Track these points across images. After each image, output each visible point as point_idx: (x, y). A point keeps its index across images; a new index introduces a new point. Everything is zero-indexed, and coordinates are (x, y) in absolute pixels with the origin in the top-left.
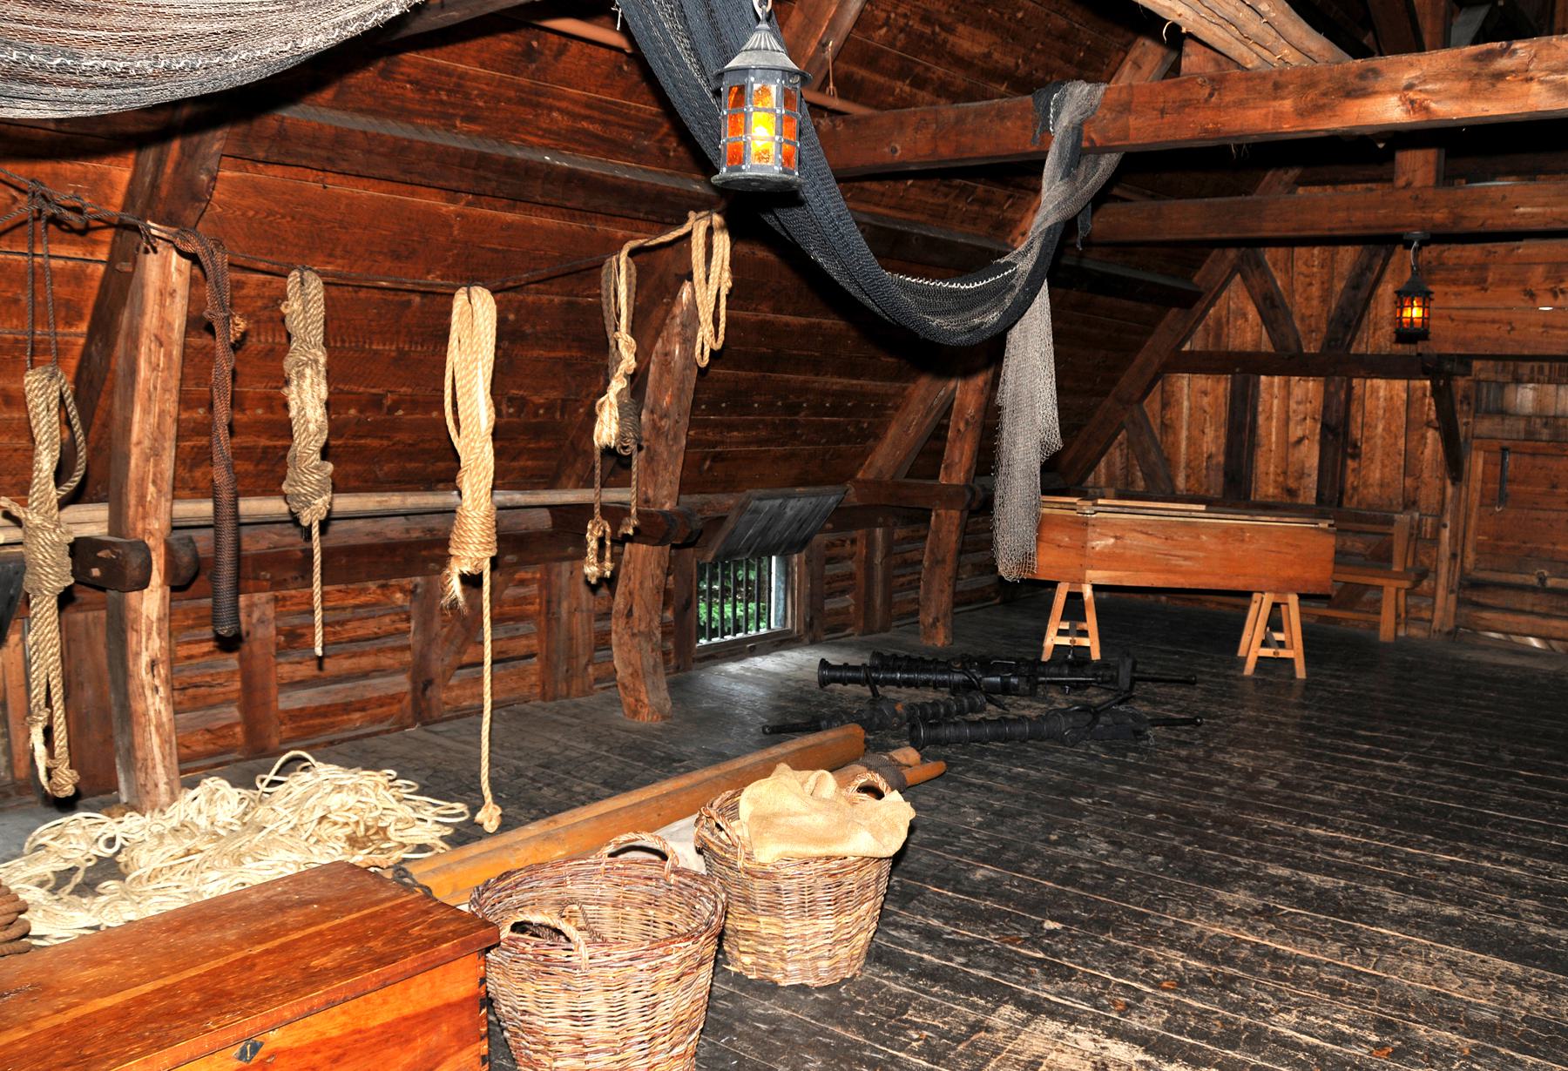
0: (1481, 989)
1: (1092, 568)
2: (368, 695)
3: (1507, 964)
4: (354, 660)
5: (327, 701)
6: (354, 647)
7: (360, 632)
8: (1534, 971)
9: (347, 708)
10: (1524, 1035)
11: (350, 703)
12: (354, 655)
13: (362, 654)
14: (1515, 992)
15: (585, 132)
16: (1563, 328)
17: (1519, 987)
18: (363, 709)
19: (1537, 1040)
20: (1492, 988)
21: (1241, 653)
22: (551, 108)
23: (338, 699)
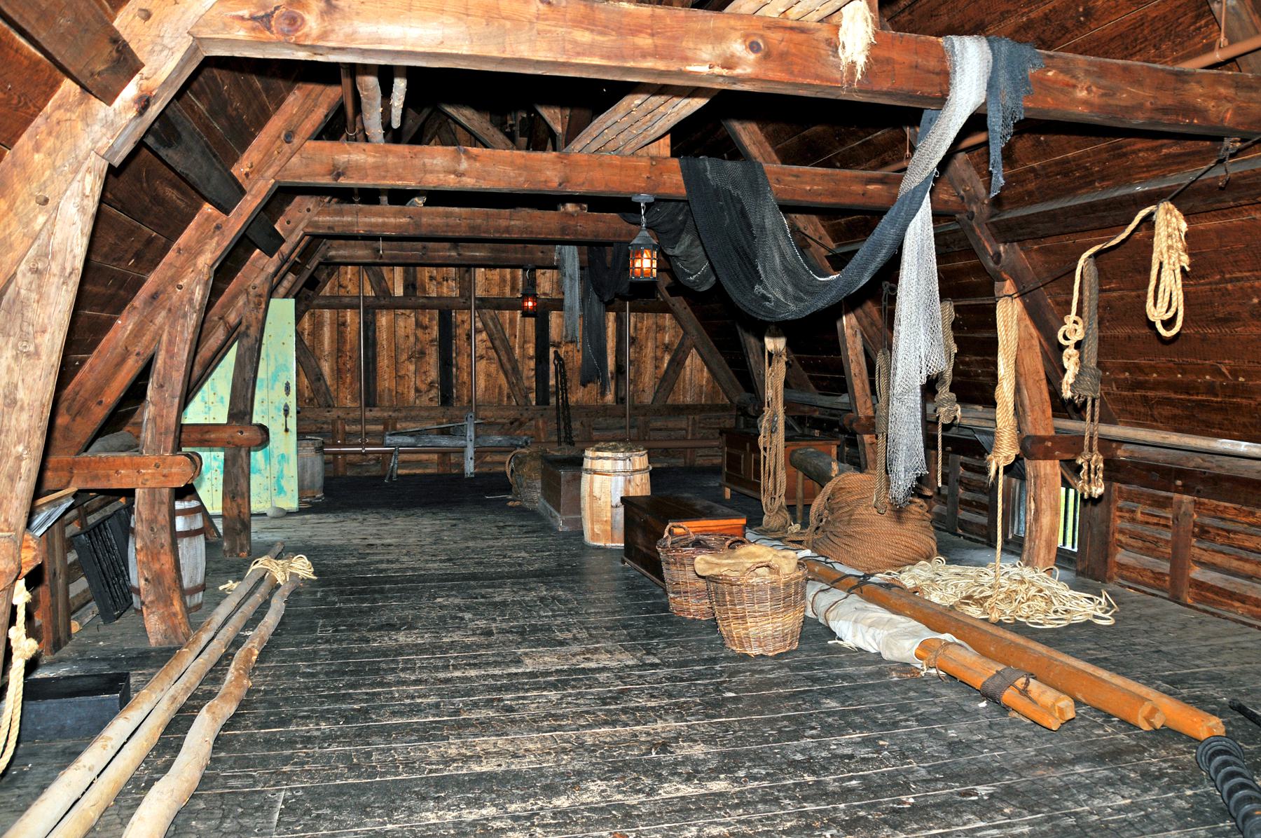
0: (484, 746)
1: (982, 526)
2: (1249, 594)
3: (484, 769)
4: (1241, 563)
5: (1220, 584)
6: (1243, 554)
7: (1247, 544)
8: (465, 771)
9: (1231, 595)
10: (441, 729)
11: (1234, 594)
12: (1240, 559)
13: (1247, 561)
14: (463, 751)
15: (1167, 156)
16: (1252, 140)
17: (465, 756)
18: (1243, 602)
19: (434, 728)
20: (478, 748)
21: (240, 170)
22: (1134, 152)
23: (1230, 587)
